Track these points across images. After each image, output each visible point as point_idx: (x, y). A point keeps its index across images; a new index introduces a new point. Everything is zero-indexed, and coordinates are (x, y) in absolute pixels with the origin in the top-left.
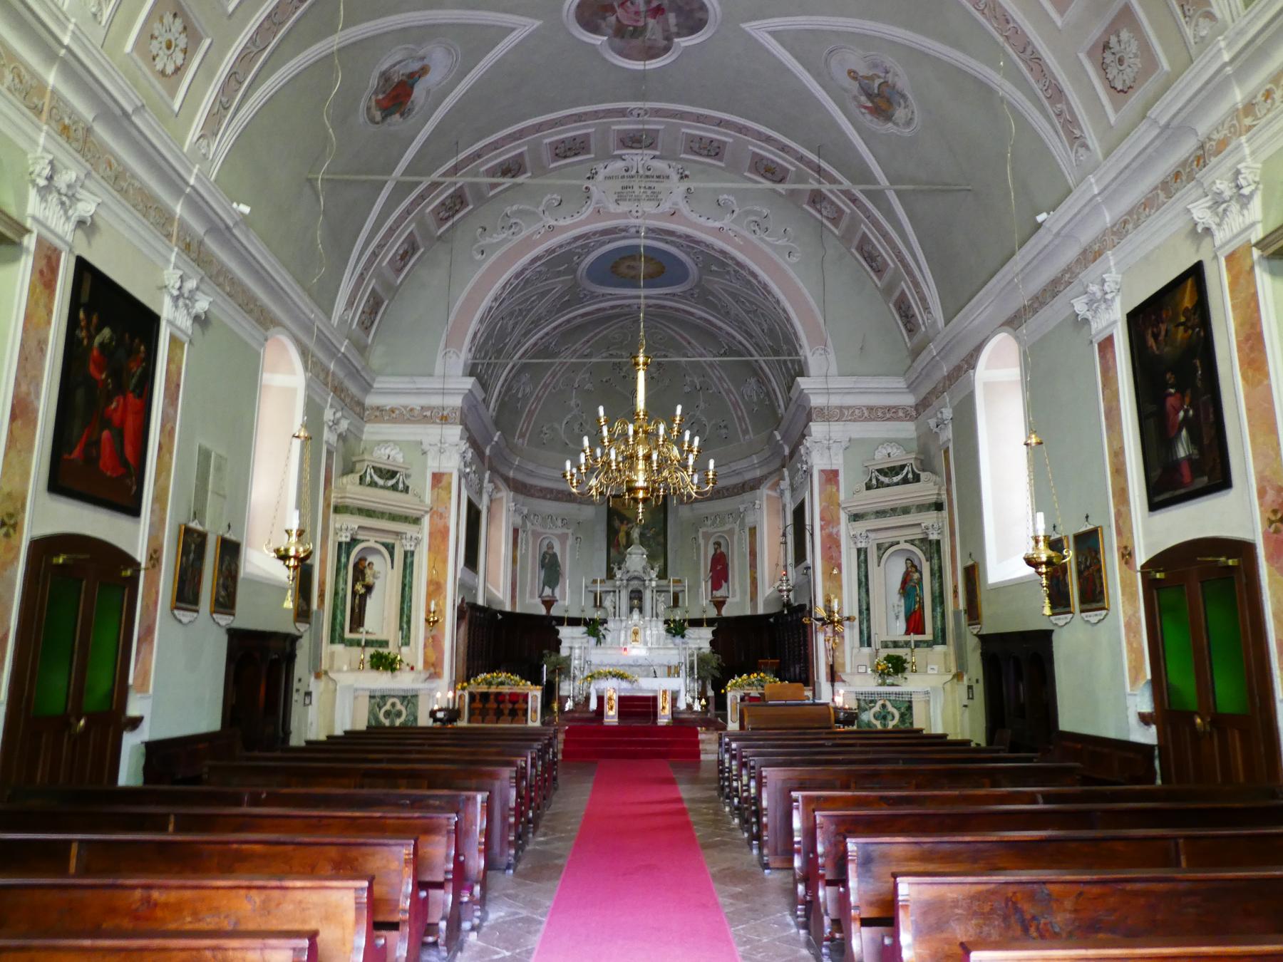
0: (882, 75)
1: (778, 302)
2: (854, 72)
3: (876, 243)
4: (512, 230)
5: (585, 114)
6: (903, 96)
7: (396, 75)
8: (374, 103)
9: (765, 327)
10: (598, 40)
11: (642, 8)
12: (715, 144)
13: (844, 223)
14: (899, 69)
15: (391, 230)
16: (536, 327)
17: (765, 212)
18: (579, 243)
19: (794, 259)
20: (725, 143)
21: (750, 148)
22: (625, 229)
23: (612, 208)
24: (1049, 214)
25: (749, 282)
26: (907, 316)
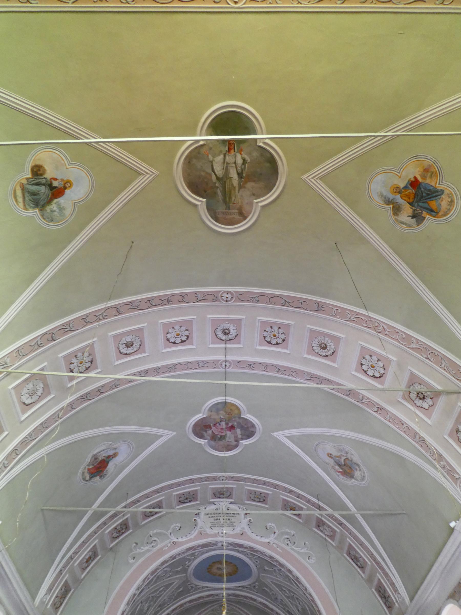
0: (345, 455)
1: (306, 589)
2: (330, 454)
3: (357, 549)
4: (152, 544)
5: (195, 479)
6: (358, 465)
7: (101, 457)
8: (86, 470)
9: (300, 608)
10: (202, 442)
11: (224, 427)
12: (263, 495)
13: (338, 537)
14: (353, 452)
15: (84, 543)
16: (161, 609)
17: (293, 532)
18: (190, 552)
19: (312, 561)
20: (268, 494)
21: (281, 496)
22: (216, 544)
23: (209, 531)
24: (456, 522)
25: (288, 576)
26: (385, 597)
